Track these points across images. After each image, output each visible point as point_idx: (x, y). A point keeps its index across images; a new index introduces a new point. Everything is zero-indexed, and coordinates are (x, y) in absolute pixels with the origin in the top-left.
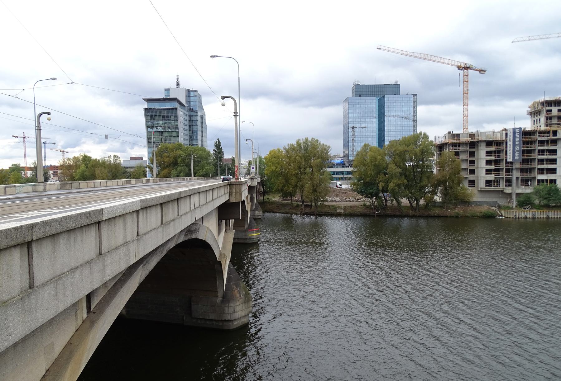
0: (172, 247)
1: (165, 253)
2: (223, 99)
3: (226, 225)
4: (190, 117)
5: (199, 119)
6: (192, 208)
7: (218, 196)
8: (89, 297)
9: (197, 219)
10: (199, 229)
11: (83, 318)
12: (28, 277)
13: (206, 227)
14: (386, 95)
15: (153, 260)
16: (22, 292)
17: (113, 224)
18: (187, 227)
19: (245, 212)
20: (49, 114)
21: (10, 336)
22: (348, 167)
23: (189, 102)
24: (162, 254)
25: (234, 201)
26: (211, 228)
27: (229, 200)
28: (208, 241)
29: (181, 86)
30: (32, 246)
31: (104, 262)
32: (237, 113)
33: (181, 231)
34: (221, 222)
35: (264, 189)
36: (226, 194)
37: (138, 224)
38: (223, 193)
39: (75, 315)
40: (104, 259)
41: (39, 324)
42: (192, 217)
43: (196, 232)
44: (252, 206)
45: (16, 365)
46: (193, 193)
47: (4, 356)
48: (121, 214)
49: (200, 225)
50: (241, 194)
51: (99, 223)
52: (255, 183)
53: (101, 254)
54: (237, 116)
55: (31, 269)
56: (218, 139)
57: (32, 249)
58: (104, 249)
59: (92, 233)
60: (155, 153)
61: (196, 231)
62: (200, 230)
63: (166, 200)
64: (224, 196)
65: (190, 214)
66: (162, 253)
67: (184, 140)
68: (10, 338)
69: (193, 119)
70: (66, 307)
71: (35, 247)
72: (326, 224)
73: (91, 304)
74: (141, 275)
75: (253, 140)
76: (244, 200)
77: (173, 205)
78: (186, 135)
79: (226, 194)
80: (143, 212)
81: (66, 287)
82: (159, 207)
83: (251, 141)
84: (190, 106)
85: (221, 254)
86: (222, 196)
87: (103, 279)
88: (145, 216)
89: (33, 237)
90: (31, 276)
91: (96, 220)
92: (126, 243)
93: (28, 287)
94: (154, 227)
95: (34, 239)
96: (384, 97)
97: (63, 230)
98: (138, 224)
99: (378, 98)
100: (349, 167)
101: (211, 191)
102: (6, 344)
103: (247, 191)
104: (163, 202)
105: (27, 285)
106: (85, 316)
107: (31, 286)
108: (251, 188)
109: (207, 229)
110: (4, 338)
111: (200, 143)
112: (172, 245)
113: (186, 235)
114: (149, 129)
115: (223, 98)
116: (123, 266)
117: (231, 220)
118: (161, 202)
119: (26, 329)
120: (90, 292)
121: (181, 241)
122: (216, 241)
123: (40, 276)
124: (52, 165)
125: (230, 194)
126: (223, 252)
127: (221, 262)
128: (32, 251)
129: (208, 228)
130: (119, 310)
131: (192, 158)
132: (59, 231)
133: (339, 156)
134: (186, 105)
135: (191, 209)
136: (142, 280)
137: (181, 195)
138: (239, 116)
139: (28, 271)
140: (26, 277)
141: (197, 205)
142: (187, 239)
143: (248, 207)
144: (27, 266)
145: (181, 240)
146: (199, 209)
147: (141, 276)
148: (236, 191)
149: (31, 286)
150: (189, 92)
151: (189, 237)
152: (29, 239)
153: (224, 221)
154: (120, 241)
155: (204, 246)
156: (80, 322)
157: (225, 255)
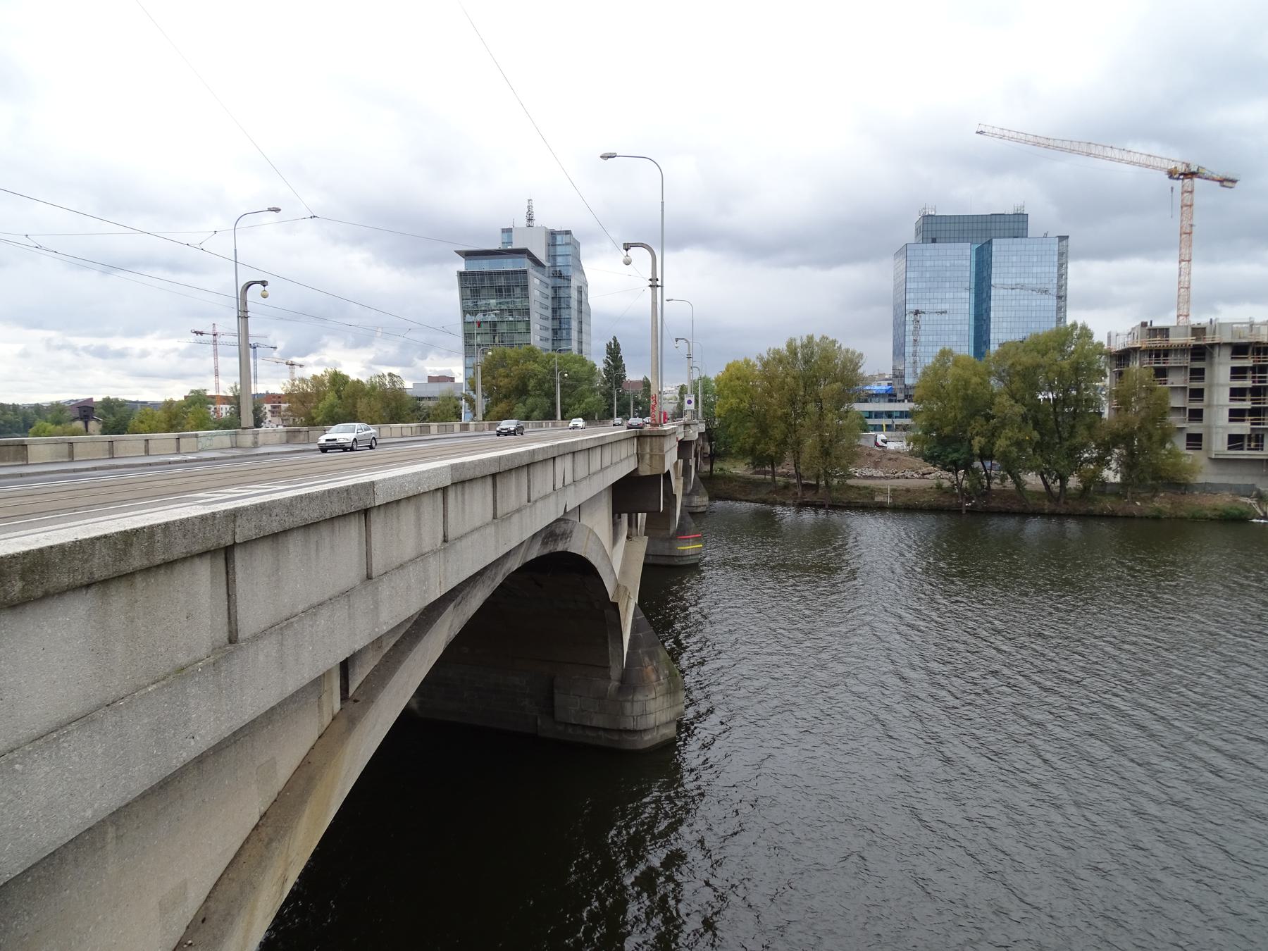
1: (499, 580)
2: (627, 250)
3: (630, 525)
4: (556, 289)
5: (574, 294)
6: (559, 485)
8: (345, 667)
9: (568, 510)
10: (571, 532)
14: (995, 237)
15: (476, 595)
18: (547, 527)
19: (670, 497)
20: (264, 283)
23: (552, 257)
27: (636, 470)
28: (590, 559)
29: (536, 223)
32: (657, 280)
33: (535, 536)
34: (620, 517)
36: (631, 456)
38: (624, 455)
43: (566, 539)
44: (685, 484)
45: (203, 801)
47: (179, 782)
50: (662, 458)
51: (366, 512)
52: (693, 434)
54: (658, 286)
55: (232, 604)
56: (615, 339)
57: (234, 561)
59: (353, 530)
61: (565, 535)
62: (574, 534)
64: (626, 462)
65: (553, 498)
66: (493, 580)
68: (193, 743)
69: (562, 293)
71: (239, 556)
73: (350, 682)
74: (451, 626)
76: (669, 471)
78: (547, 329)
79: (631, 456)
83: (687, 342)
84: (554, 266)
85: (618, 587)
86: (621, 461)
92: (421, 556)
93: (227, 641)
95: (237, 541)
96: (990, 242)
97: (296, 525)
99: (977, 246)
100: (906, 401)
101: (598, 450)
103: (675, 451)
104: (498, 470)
105: (223, 635)
106: (337, 706)
107: (233, 639)
111: (574, 346)
112: (514, 564)
113: (544, 543)
114: (468, 316)
115: (627, 247)
116: (414, 606)
117: (640, 514)
119: (223, 727)
122: (608, 559)
123: (249, 622)
124: (270, 392)
125: (640, 457)
126: (623, 583)
129: (591, 531)
131: (558, 378)
132: (287, 526)
134: (547, 264)
135: (557, 487)
137: (536, 457)
138: (662, 286)
139: (226, 607)
140: (222, 619)
141: (569, 480)
142: (546, 551)
143: (677, 486)
145: (534, 553)
148: (651, 450)
149: (233, 639)
150: (553, 234)
151: (550, 548)
152: (228, 540)
153: (625, 517)
154: (409, 551)
155: (582, 569)
156: (327, 720)
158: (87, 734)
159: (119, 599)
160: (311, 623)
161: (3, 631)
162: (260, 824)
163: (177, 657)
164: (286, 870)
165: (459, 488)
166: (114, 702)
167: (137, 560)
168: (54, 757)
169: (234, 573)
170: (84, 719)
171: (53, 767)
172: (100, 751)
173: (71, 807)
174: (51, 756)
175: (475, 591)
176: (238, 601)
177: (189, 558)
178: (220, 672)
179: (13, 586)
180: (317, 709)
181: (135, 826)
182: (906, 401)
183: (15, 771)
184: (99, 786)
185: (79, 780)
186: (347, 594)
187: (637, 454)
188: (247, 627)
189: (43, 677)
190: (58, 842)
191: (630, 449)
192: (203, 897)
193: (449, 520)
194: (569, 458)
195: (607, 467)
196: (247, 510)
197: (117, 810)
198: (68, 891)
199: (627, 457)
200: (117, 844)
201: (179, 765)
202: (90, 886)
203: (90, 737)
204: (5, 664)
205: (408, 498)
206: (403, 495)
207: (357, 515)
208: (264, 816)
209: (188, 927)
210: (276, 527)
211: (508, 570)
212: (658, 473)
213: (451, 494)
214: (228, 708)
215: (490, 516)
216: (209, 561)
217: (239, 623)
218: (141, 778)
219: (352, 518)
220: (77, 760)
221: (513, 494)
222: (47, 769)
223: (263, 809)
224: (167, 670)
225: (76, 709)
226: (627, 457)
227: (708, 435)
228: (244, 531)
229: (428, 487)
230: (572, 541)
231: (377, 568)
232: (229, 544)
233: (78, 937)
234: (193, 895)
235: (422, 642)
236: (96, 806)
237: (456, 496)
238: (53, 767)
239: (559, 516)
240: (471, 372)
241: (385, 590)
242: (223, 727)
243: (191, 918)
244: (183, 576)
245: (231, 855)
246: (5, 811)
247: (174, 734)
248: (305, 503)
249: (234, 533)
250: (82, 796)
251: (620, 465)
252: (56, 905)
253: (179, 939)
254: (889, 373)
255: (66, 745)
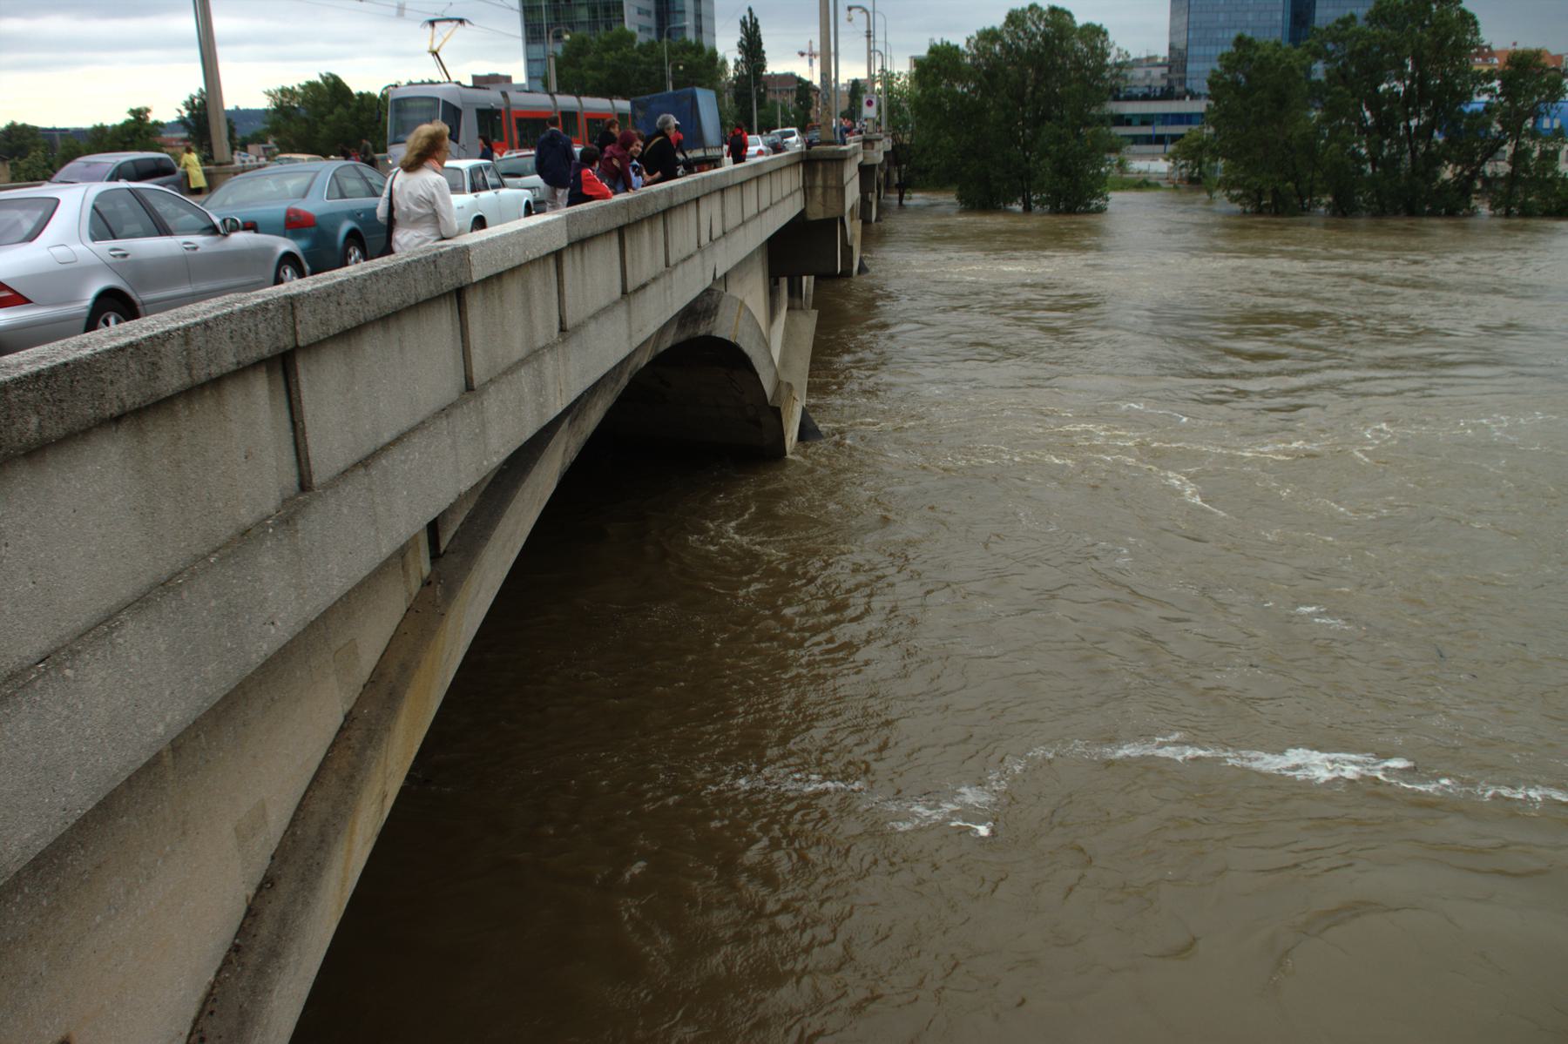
0: (645, 362)
3: (791, 294)
6: (705, 239)
7: (774, 200)
9: (718, 276)
10: (717, 307)
11: (421, 572)
12: (293, 458)
13: (737, 299)
15: (596, 405)
16: (284, 501)
17: (496, 296)
21: (272, 627)
22: (1184, 98)
24: (619, 387)
25: (821, 216)
26: (748, 302)
27: (802, 213)
28: (742, 345)
30: (295, 365)
31: (482, 412)
34: (777, 283)
35: (903, 175)
36: (796, 191)
37: (560, 293)
38: (786, 191)
39: (400, 565)
40: (482, 404)
41: (336, 594)
42: (704, 269)
43: (710, 317)
45: (272, 700)
46: (707, 191)
48: (517, 263)
49: (719, 293)
51: (459, 295)
52: (878, 156)
53: (473, 390)
55: (300, 434)
56: (750, 10)
57: (296, 375)
58: (479, 374)
59: (443, 321)
60: (552, 61)
62: (721, 311)
63: (634, 216)
64: (789, 202)
65: (697, 260)
66: (618, 381)
67: (639, 13)
68: (273, 631)
70: (399, 546)
72: (899, 276)
73: (440, 534)
74: (566, 450)
75: (870, 9)
77: (652, 232)
79: (796, 191)
80: (573, 254)
81: (392, 487)
82: (615, 239)
83: (865, 10)
85: (778, 384)
86: (783, 199)
87: (482, 463)
88: (579, 270)
89: (300, 337)
90: (302, 456)
91: (449, 283)
92: (534, 355)
93: (297, 488)
94: (604, 302)
95: (301, 344)
97: (370, 316)
98: (560, 293)
100: (1188, 98)
101: (754, 184)
102: (265, 647)
104: (626, 221)
105: (291, 479)
106: (426, 568)
107: (305, 485)
108: (865, 171)
109: (741, 307)
110: (258, 630)
111: (689, 22)
117: (805, 278)
118: (621, 220)
119: (308, 608)
120: (452, 501)
121: (668, 345)
122: (766, 344)
123: (328, 455)
124: (241, 108)
125: (808, 190)
126: (785, 378)
127: (779, 409)
128: (297, 381)
130: (512, 552)
131: (669, 70)
133: (1150, 61)
135: (702, 243)
136: (568, 462)
137: (675, 199)
139: (290, 441)
140: (289, 457)
141: (717, 232)
142: (683, 337)
144: (288, 425)
145: (667, 342)
146: (722, 241)
147: (564, 454)
148: (825, 180)
149: (305, 485)
153: (784, 282)
154: (518, 349)
155: (732, 358)
156: (415, 586)
157: (789, 385)
158: (144, 625)
159: (158, 436)
160: (403, 458)
161: (22, 489)
162: (346, 725)
163: (240, 514)
164: (385, 783)
165: (577, 251)
166: (169, 580)
167: (172, 380)
168: (109, 657)
169: (298, 391)
170: (140, 602)
171: (110, 671)
172: (163, 647)
173: (138, 721)
174: (105, 657)
175: (595, 399)
176: (307, 430)
177: (241, 372)
178: (297, 531)
179: (27, 423)
180: (401, 572)
181: (193, 735)
182: (1188, 98)
183: (65, 678)
184: (167, 693)
185: (142, 686)
186: (445, 411)
187: (804, 186)
188: (322, 471)
189: (79, 549)
190: (131, 768)
191: (791, 181)
192: (286, 821)
193: (567, 299)
194: (717, 198)
195: (766, 210)
196: (309, 295)
197: (195, 723)
198: (125, 818)
199: (791, 194)
200: (174, 757)
201: (260, 661)
202: (150, 811)
203: (148, 628)
204: (31, 535)
205: (513, 270)
206: (508, 265)
207: (448, 298)
208: (349, 717)
209: (273, 858)
210: (349, 322)
211: (637, 365)
212: (835, 216)
213: (567, 260)
214: (311, 581)
215: (618, 293)
216: (265, 375)
217: (312, 463)
218: (216, 679)
219: (442, 301)
220: (137, 659)
221: (646, 254)
222: (103, 674)
223: (347, 708)
224: (230, 533)
225: (125, 591)
226: (791, 194)
227: (893, 157)
228: (309, 330)
229: (538, 251)
230: (718, 321)
231: (479, 376)
232: (289, 347)
233: (145, 873)
234: (274, 818)
235: (532, 475)
236: (168, 718)
237: (574, 262)
238: (110, 671)
239: (707, 286)
240: (537, 67)
241: (492, 402)
242: (308, 608)
243: (275, 846)
244: (234, 397)
245: (314, 767)
246: (63, 730)
247: (249, 620)
248: (382, 283)
249: (295, 333)
250: (150, 707)
251: (781, 205)
252: (113, 835)
253: (264, 872)
254: (1163, 52)
255: (120, 641)
